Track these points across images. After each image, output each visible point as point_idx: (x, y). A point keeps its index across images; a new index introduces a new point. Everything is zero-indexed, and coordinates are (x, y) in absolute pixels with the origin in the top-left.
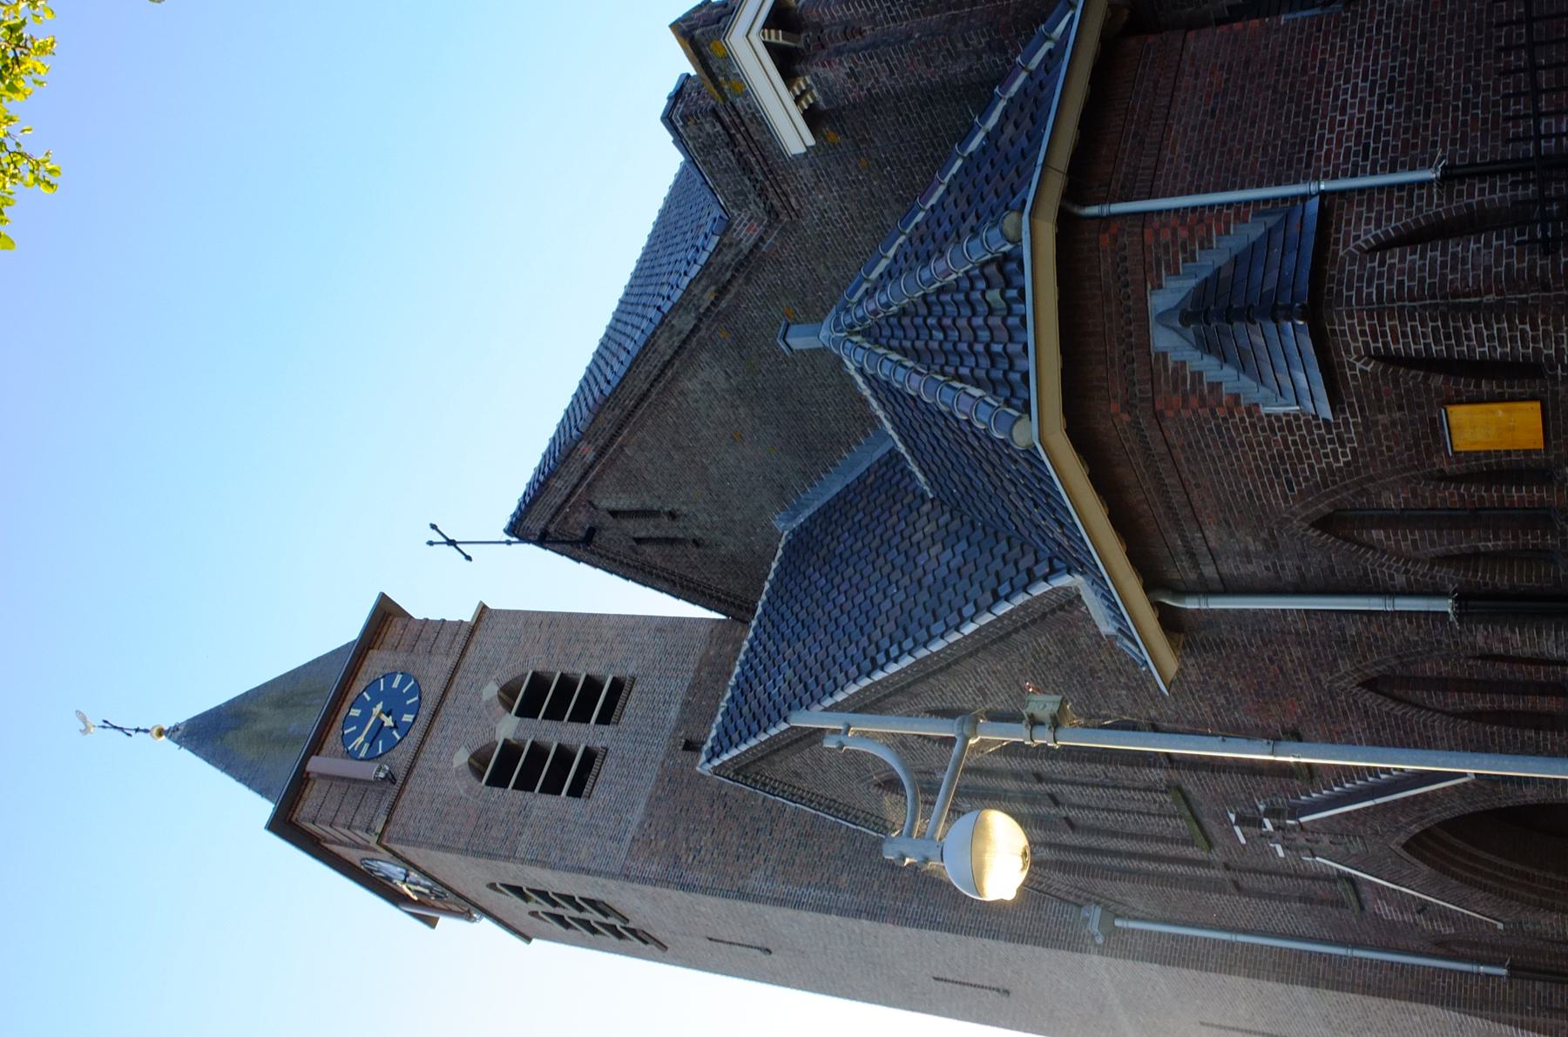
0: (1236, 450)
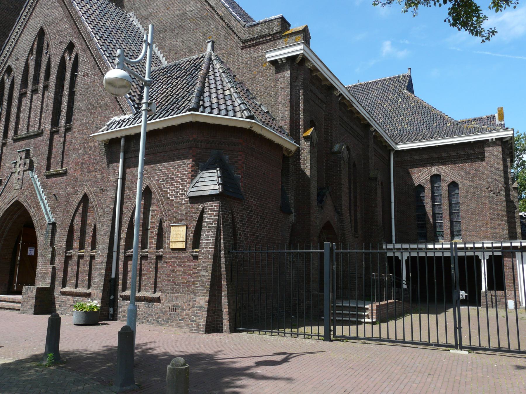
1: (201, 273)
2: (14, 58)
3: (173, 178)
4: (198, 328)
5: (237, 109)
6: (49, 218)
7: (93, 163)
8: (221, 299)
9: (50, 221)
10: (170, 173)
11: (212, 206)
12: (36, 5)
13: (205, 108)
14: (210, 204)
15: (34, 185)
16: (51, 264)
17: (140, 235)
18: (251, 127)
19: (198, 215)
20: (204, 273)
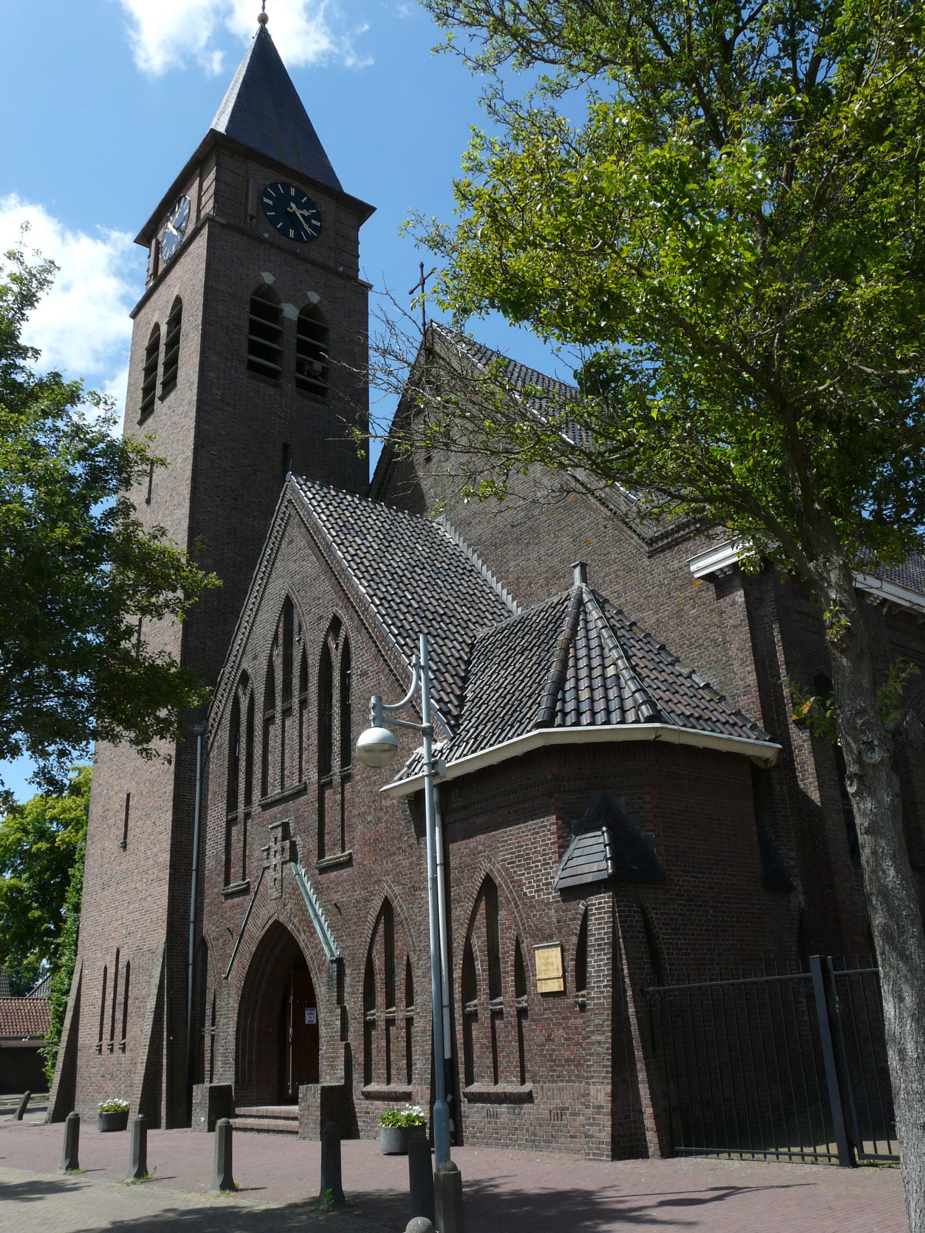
0: (532, 835)
1: (594, 1038)
2: (250, 655)
3: (528, 854)
4: (599, 1149)
5: (629, 704)
6: (330, 950)
7: (393, 838)
8: (638, 1089)
9: (332, 955)
10: (522, 846)
11: (600, 903)
12: (276, 556)
13: (565, 715)
14: (596, 899)
15: (301, 888)
16: (342, 1040)
17: (486, 969)
18: (656, 737)
19: (579, 922)
20: (599, 1038)
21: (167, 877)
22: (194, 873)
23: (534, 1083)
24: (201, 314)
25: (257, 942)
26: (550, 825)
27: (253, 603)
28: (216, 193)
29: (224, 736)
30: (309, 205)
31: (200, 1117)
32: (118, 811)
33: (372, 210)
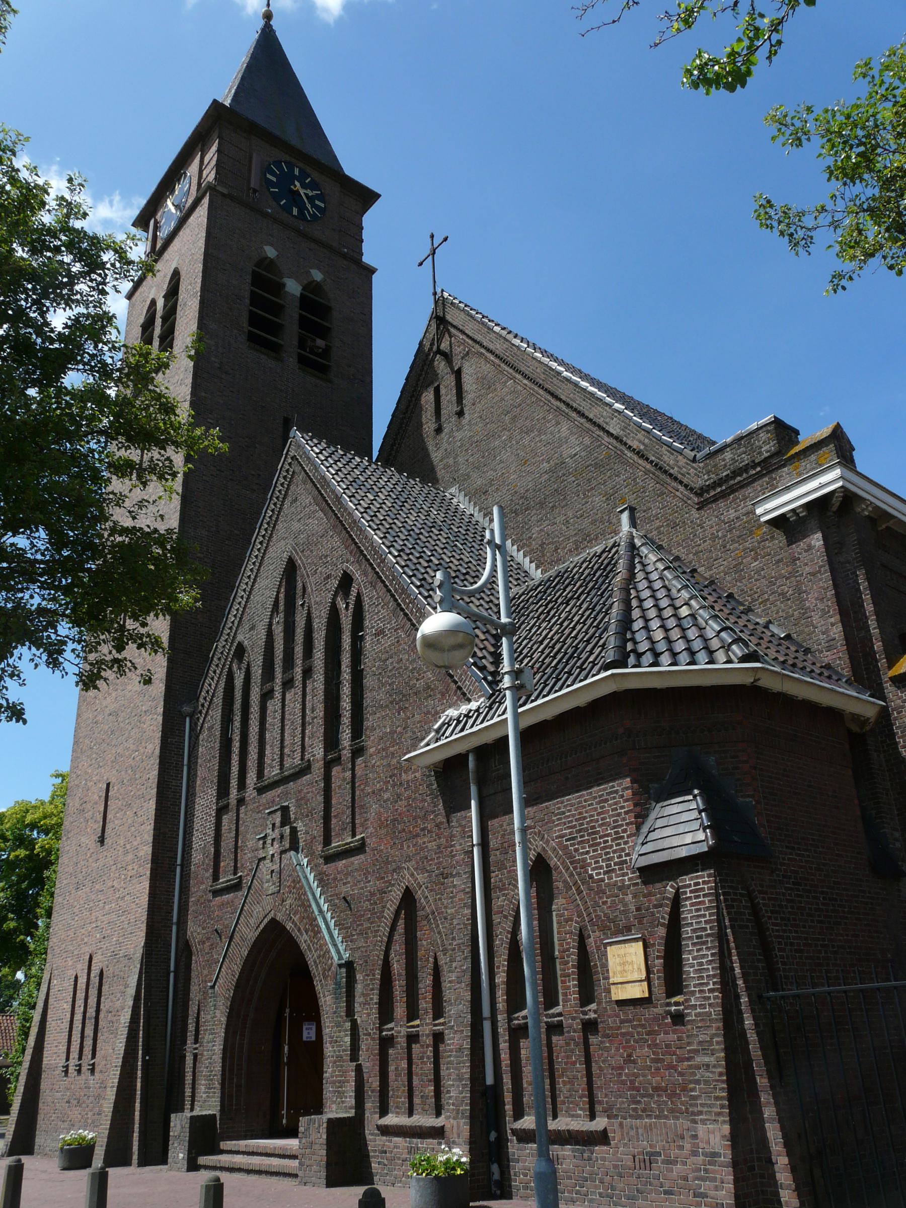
2: (247, 627)
6: (338, 952)
7: (415, 818)
9: (340, 958)
10: (585, 818)
11: (697, 884)
13: (639, 655)
14: (691, 879)
15: (303, 880)
18: (755, 681)
19: (668, 909)
20: (706, 1059)
21: (148, 873)
22: (178, 869)
23: (609, 1117)
24: (199, 281)
25: (250, 944)
26: (623, 790)
27: (251, 570)
28: (218, 165)
29: (216, 715)
30: (314, 186)
31: (178, 1153)
32: (96, 803)
33: (378, 196)
